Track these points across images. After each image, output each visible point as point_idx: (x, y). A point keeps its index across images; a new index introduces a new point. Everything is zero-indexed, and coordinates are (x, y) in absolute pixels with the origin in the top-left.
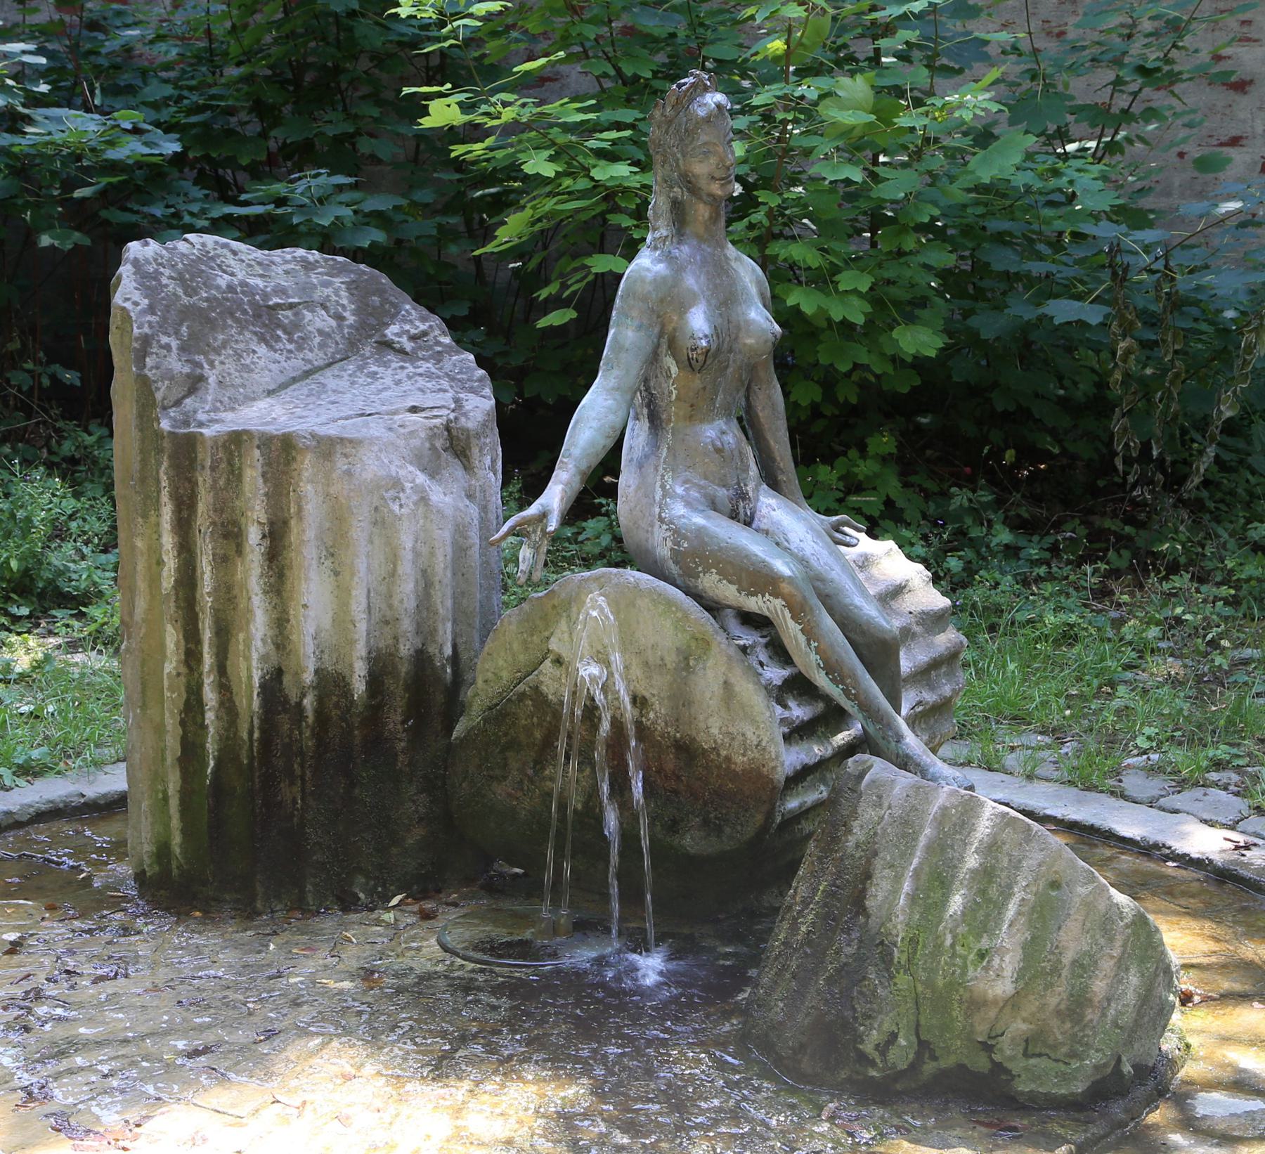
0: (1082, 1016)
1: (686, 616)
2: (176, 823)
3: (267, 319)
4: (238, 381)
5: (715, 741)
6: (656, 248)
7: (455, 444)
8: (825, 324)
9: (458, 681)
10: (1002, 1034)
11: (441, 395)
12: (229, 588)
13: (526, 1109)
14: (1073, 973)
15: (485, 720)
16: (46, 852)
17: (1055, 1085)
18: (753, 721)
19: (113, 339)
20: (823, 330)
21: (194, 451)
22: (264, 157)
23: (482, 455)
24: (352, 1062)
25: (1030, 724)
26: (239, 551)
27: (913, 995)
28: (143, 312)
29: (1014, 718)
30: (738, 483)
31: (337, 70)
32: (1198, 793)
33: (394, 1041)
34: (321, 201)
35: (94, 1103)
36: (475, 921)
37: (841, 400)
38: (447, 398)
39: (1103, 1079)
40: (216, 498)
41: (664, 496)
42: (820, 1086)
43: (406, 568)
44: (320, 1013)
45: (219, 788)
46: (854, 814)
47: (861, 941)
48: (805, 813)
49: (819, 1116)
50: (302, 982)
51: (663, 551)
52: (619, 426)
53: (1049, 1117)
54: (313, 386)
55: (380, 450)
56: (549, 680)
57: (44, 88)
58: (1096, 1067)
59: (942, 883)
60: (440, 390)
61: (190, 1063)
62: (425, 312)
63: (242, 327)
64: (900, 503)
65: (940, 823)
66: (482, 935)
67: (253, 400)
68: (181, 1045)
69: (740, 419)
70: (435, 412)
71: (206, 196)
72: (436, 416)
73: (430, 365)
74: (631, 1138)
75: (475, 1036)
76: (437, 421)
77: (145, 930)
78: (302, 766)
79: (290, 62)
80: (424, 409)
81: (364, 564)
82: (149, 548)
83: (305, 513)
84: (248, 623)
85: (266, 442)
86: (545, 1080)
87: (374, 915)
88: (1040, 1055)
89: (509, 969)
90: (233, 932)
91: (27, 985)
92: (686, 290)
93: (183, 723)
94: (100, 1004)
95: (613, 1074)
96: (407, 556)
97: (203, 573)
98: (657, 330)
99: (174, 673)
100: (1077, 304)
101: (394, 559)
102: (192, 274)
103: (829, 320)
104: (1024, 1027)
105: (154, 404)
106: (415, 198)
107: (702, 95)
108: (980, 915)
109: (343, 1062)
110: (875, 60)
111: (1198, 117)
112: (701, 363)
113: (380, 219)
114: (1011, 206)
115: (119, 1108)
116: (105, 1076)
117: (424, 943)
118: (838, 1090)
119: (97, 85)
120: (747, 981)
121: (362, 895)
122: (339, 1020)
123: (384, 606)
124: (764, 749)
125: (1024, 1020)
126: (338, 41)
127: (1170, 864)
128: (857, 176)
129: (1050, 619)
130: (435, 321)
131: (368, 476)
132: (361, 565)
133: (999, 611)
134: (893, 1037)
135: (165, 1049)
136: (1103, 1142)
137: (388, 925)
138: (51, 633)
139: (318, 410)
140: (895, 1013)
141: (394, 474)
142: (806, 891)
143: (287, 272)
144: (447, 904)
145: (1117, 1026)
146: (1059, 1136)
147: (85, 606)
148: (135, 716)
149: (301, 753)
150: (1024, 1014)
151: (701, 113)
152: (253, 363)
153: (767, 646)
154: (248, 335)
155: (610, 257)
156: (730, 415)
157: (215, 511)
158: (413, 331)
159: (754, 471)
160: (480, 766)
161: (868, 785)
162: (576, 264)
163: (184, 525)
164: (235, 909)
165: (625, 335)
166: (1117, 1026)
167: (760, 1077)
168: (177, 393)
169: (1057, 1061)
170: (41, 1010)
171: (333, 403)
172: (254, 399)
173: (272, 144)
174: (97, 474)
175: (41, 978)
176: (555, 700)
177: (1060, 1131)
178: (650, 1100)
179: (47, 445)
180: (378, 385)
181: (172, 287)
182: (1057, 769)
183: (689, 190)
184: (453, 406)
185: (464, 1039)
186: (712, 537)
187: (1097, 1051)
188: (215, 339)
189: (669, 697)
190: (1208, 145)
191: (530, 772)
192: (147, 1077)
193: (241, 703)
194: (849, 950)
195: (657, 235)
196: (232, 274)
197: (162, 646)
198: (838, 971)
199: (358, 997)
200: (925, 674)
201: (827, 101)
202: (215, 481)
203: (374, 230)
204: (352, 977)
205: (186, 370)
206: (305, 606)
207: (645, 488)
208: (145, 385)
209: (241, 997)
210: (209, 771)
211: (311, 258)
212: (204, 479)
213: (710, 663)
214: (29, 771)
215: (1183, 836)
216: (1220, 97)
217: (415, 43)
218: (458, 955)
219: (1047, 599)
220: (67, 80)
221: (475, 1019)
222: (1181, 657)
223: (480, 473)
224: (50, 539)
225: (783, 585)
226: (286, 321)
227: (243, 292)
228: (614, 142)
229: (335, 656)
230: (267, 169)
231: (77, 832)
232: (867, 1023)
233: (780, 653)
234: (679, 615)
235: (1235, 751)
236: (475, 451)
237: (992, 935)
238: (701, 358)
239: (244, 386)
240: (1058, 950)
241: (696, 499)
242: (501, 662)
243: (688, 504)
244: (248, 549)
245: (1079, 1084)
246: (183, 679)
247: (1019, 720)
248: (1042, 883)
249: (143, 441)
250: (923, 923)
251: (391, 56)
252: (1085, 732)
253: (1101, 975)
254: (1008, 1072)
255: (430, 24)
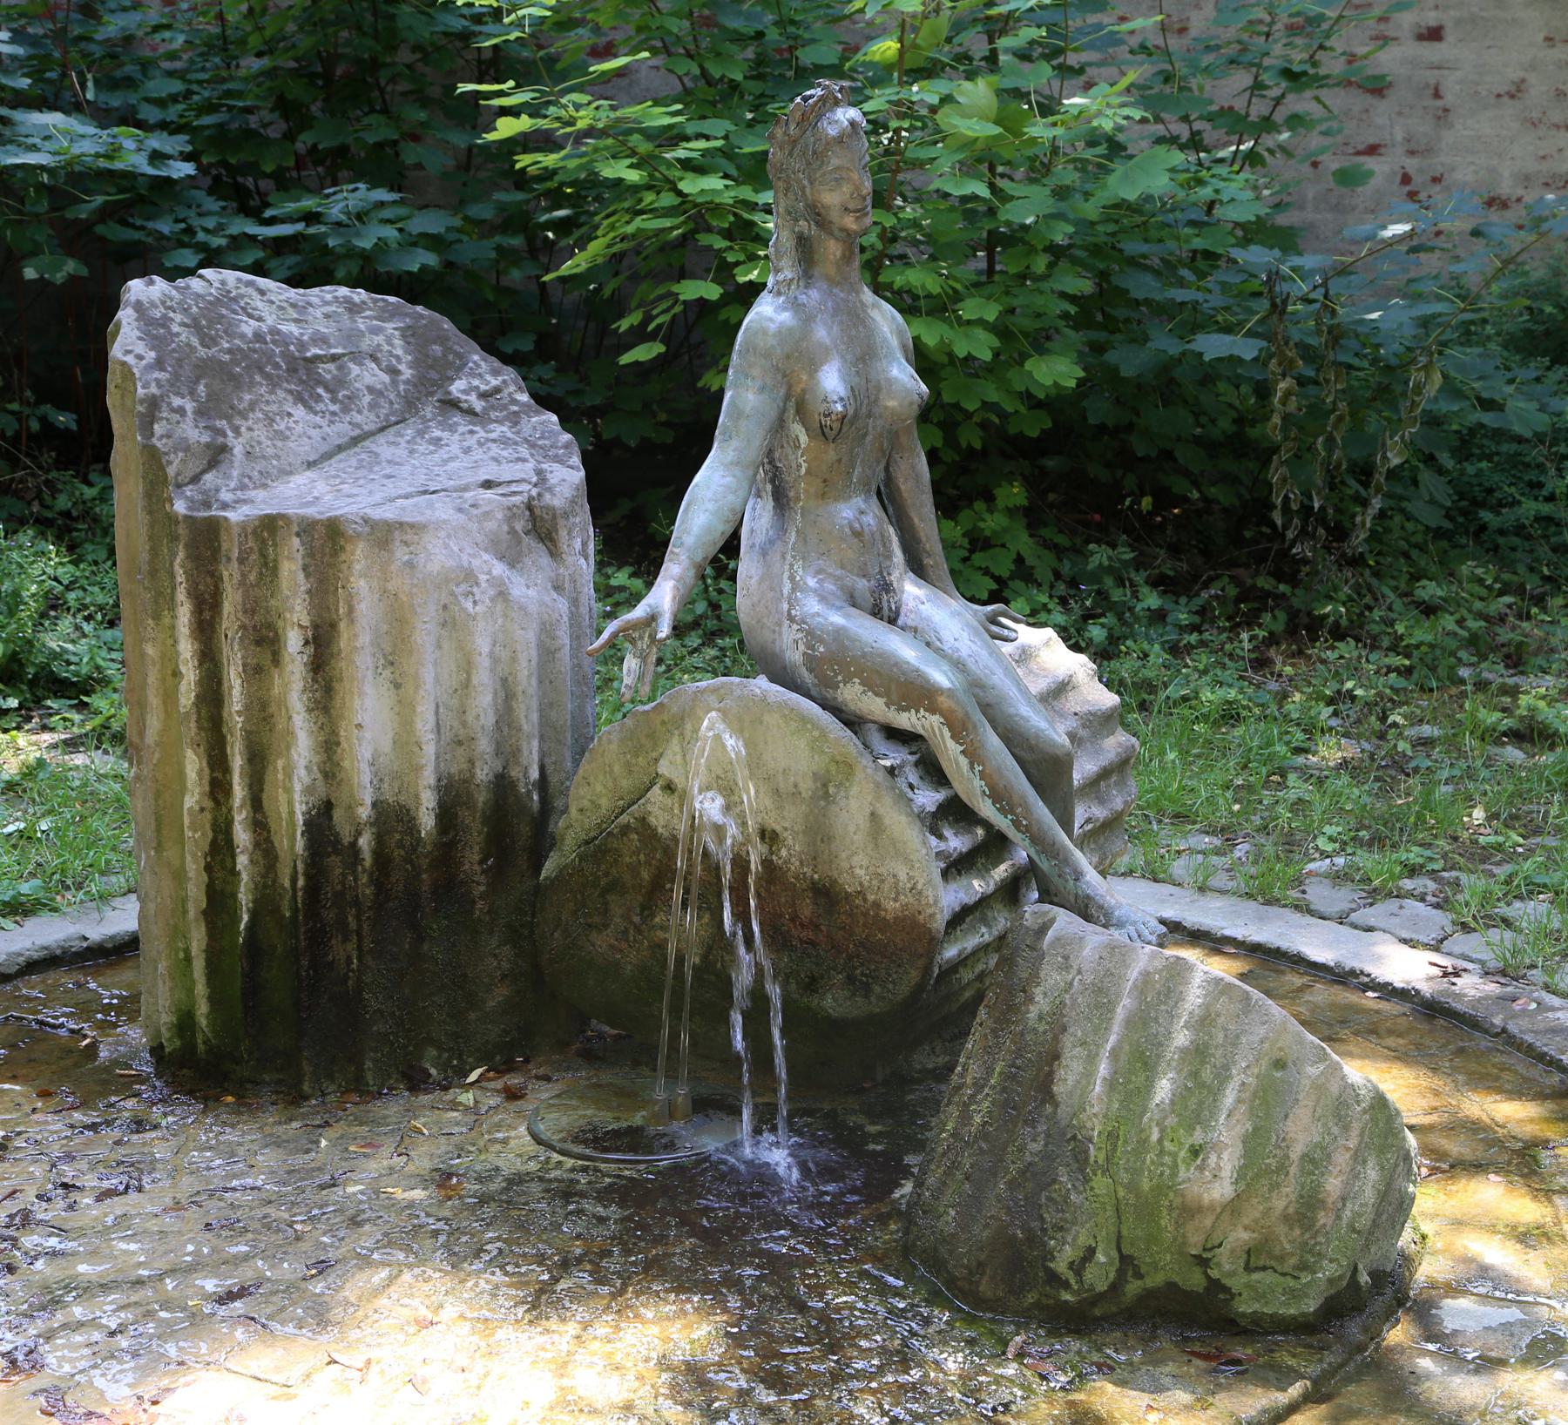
0: (1313, 1220)
1: (824, 734)
2: (201, 989)
3: (305, 373)
4: (270, 451)
5: (861, 884)
6: (779, 294)
7: (539, 526)
8: (945, 360)
9: (547, 809)
10: (1220, 1245)
11: (519, 466)
12: (264, 706)
13: (647, 1360)
14: (1302, 1170)
15: (581, 857)
16: (39, 1012)
17: (1283, 1304)
18: (907, 860)
19: (112, 400)
20: (943, 366)
21: (217, 538)
22: (291, 163)
23: (571, 538)
24: (427, 1302)
25: (1194, 823)
26: (276, 660)
27: (1114, 1201)
28: (150, 367)
29: (1177, 816)
30: (881, 573)
31: (375, 65)
32: (1393, 904)
33: (479, 1271)
34: (359, 217)
35: (97, 1372)
36: (574, 1102)
37: (964, 445)
38: (527, 470)
39: (1338, 1293)
40: (246, 596)
41: (794, 590)
42: (1002, 1313)
43: (483, 677)
44: (386, 1234)
45: (254, 947)
46: (1034, 977)
47: (1048, 1136)
48: (963, 961)
49: (1004, 1353)
50: (362, 1193)
51: (794, 655)
52: (738, 508)
53: (1276, 1343)
54: (364, 456)
55: (449, 537)
56: (658, 810)
57: (24, 83)
58: (1331, 1281)
59: (1146, 1064)
60: (519, 459)
61: (223, 1311)
62: (497, 364)
63: (274, 384)
64: (1030, 561)
65: (1142, 992)
66: (582, 1122)
67: (289, 473)
68: (210, 1285)
69: (879, 493)
70: (514, 488)
71: (224, 208)
72: (514, 493)
73: (504, 429)
74: (778, 1395)
75: (579, 1260)
76: (517, 499)
77: (164, 1123)
78: (358, 918)
79: (319, 53)
80: (500, 484)
81: (431, 675)
82: (163, 656)
83: (357, 614)
84: (288, 748)
85: (307, 528)
86: (668, 1318)
87: (449, 1096)
88: (1264, 1268)
89: (616, 1166)
90: (275, 1123)
91: (12, 1207)
92: (817, 344)
93: (208, 868)
94: (107, 1230)
95: (751, 1306)
96: (484, 662)
97: (231, 688)
98: (782, 392)
99: (197, 808)
100: (1228, 338)
101: (467, 666)
102: (211, 319)
103: (951, 355)
104: (1245, 1236)
105: (165, 480)
106: (470, 214)
107: (832, 110)
108: (1192, 1103)
109: (416, 1302)
110: (992, 58)
111: (1335, 125)
112: (829, 431)
113: (432, 242)
114: (1144, 223)
115: (130, 1378)
116: (112, 1334)
117: (510, 1130)
118: (1024, 1319)
119: (89, 76)
120: (906, 1172)
121: (433, 1071)
122: (407, 1238)
123: (456, 724)
124: (920, 893)
125: (1245, 1228)
126: (376, 31)
127: (1370, 994)
128: (983, 191)
129: (1207, 695)
130: (509, 374)
131: (434, 567)
132: (428, 674)
133: (1151, 688)
134: (1091, 1252)
135: (190, 1292)
136: (1342, 1373)
137: (467, 1108)
138: (45, 728)
139: (370, 486)
140: (1092, 1223)
141: (466, 564)
142: (977, 1066)
143: (327, 316)
144: (538, 1078)
145: (1354, 1230)
146: (1291, 1369)
147: (87, 694)
148: (148, 857)
149: (356, 903)
150: (1246, 1221)
151: (832, 131)
152: (288, 428)
153: (916, 764)
154: (281, 394)
155: (700, 283)
156: (869, 491)
157: (245, 612)
158: (483, 387)
159: (898, 556)
160: (575, 912)
161: (1052, 944)
162: (661, 291)
163: (205, 628)
164: (277, 1093)
165: (744, 398)
166: (1354, 1230)
167: (929, 1303)
168: (193, 468)
169: (1284, 1275)
170: (29, 1241)
171: (389, 477)
172: (291, 473)
173: (299, 146)
174: (99, 532)
175: (31, 1194)
176: (666, 834)
177: (1292, 1362)
178: (799, 1341)
179: (39, 496)
180: (443, 453)
181: (185, 336)
182: (1232, 878)
183: (817, 223)
184: (535, 479)
185: (565, 1265)
186: (854, 641)
187: (1331, 1261)
188: (241, 400)
189: (804, 832)
190: (1344, 154)
191: (637, 919)
192: (167, 1332)
193: (282, 843)
194: (1035, 1147)
195: (780, 277)
196: (260, 319)
197: (181, 775)
198: (1022, 1173)
199: (432, 1210)
200: (1095, 785)
201: (946, 109)
202: (244, 575)
203: (420, 251)
204: (424, 1183)
205: (205, 438)
206: (359, 726)
207: (770, 580)
208: (153, 460)
209: (286, 1216)
210: (242, 927)
211: (356, 299)
212: (230, 574)
213: (854, 790)
214: (19, 909)
215: (1378, 959)
216: (1355, 101)
217: (465, 37)
218: (553, 1149)
219: (1205, 672)
220: (52, 70)
221: (578, 1237)
222: (1358, 737)
223: (570, 560)
224: (43, 615)
225: (941, 699)
226: (328, 377)
227: (274, 342)
228: (705, 153)
229: (396, 785)
230: (294, 174)
231: (79, 985)
232: (1059, 1236)
233: (933, 772)
234: (816, 733)
235: (1428, 853)
236: (563, 533)
237: (1207, 1128)
238: (836, 426)
239: (278, 457)
240: (1284, 1143)
241: (833, 594)
242: (599, 788)
243: (823, 599)
244: (287, 659)
245: (1312, 1302)
246: (208, 816)
247: (1182, 818)
248: (1264, 1063)
249: (152, 526)
250: (1124, 1113)
251: (438, 49)
252: (1258, 831)
253: (1335, 1172)
254: (1226, 1290)
255: (484, 14)
